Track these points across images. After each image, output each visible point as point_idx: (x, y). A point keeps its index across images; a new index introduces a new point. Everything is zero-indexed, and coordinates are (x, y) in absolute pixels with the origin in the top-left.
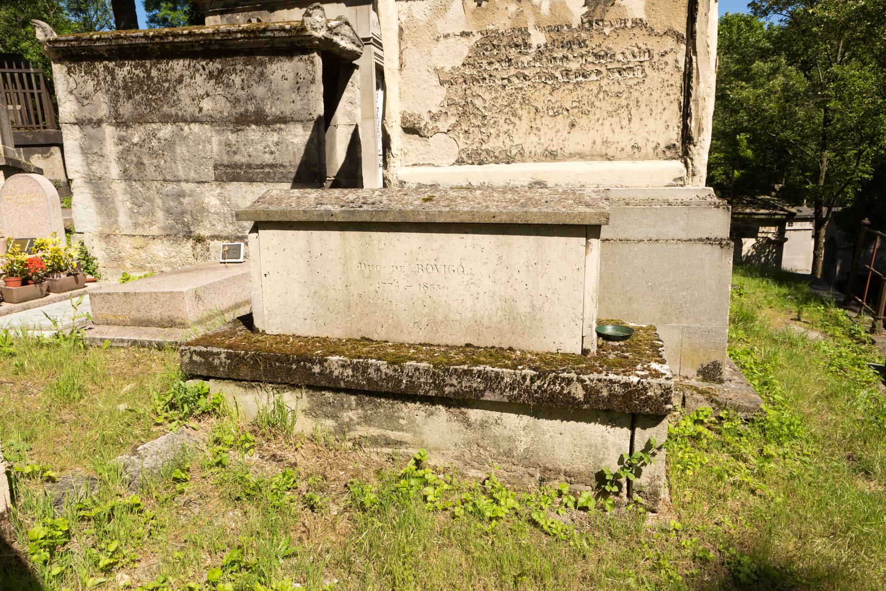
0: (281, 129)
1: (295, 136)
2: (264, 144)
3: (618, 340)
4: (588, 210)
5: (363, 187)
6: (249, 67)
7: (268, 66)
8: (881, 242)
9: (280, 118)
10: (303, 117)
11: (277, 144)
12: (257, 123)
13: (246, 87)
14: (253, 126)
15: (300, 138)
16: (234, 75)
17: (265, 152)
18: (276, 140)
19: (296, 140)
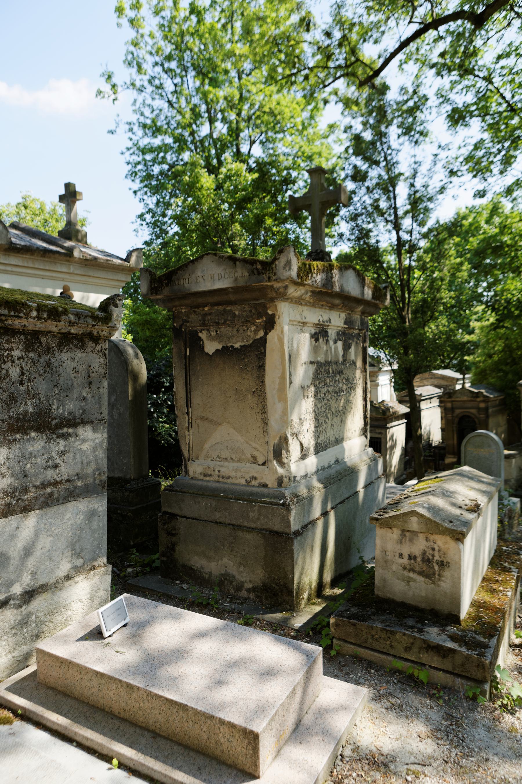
0: (69, 435)
1: (84, 441)
2: (46, 456)
3: (366, 383)
4: (258, 616)
5: (324, 674)
6: (31, 355)
7: (57, 354)
8: (392, 421)
9: (68, 420)
10: (93, 418)
11: (63, 453)
12: (39, 429)
13: (25, 382)
14: (33, 434)
15: (90, 443)
16: (9, 364)
17: (47, 467)
18: (62, 448)
19: (85, 447)
